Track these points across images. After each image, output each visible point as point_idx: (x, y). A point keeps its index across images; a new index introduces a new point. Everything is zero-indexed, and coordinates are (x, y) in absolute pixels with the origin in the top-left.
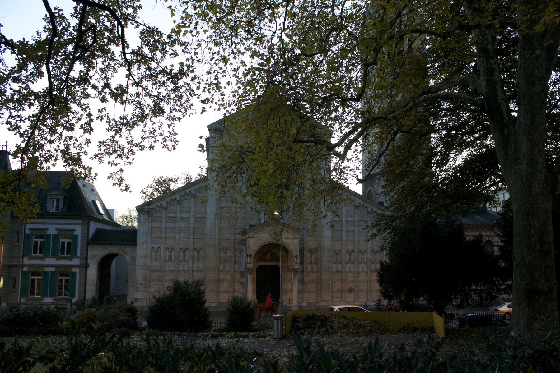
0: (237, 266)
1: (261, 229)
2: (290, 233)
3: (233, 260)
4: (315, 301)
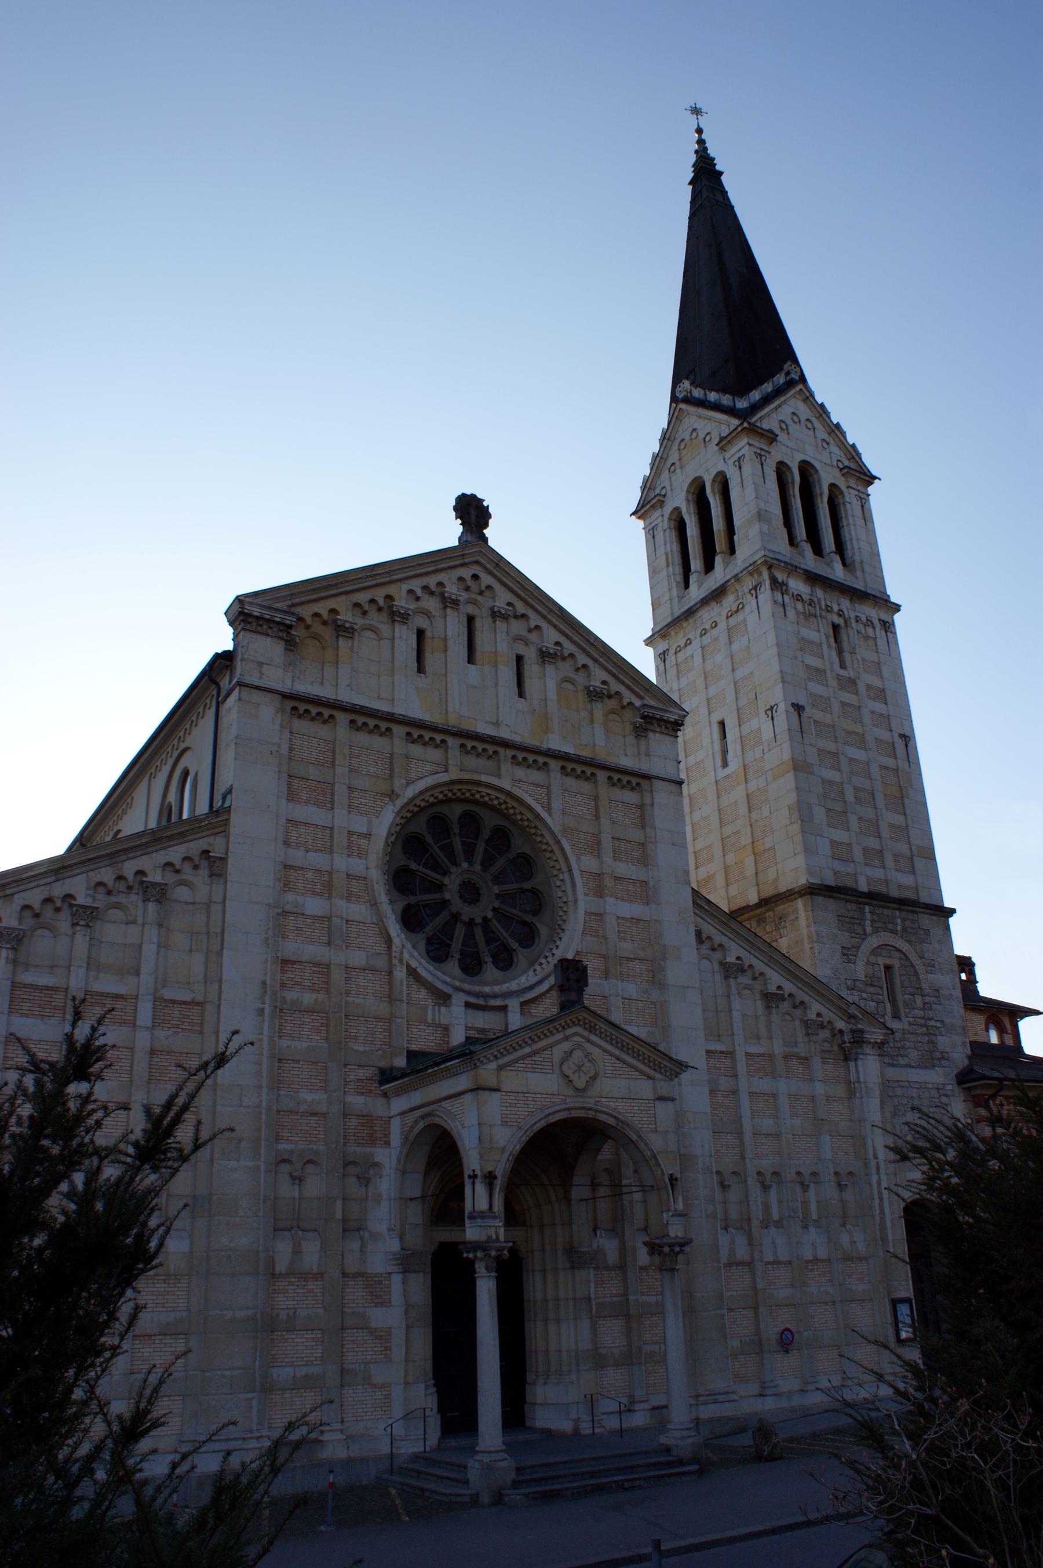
0: (356, 1245)
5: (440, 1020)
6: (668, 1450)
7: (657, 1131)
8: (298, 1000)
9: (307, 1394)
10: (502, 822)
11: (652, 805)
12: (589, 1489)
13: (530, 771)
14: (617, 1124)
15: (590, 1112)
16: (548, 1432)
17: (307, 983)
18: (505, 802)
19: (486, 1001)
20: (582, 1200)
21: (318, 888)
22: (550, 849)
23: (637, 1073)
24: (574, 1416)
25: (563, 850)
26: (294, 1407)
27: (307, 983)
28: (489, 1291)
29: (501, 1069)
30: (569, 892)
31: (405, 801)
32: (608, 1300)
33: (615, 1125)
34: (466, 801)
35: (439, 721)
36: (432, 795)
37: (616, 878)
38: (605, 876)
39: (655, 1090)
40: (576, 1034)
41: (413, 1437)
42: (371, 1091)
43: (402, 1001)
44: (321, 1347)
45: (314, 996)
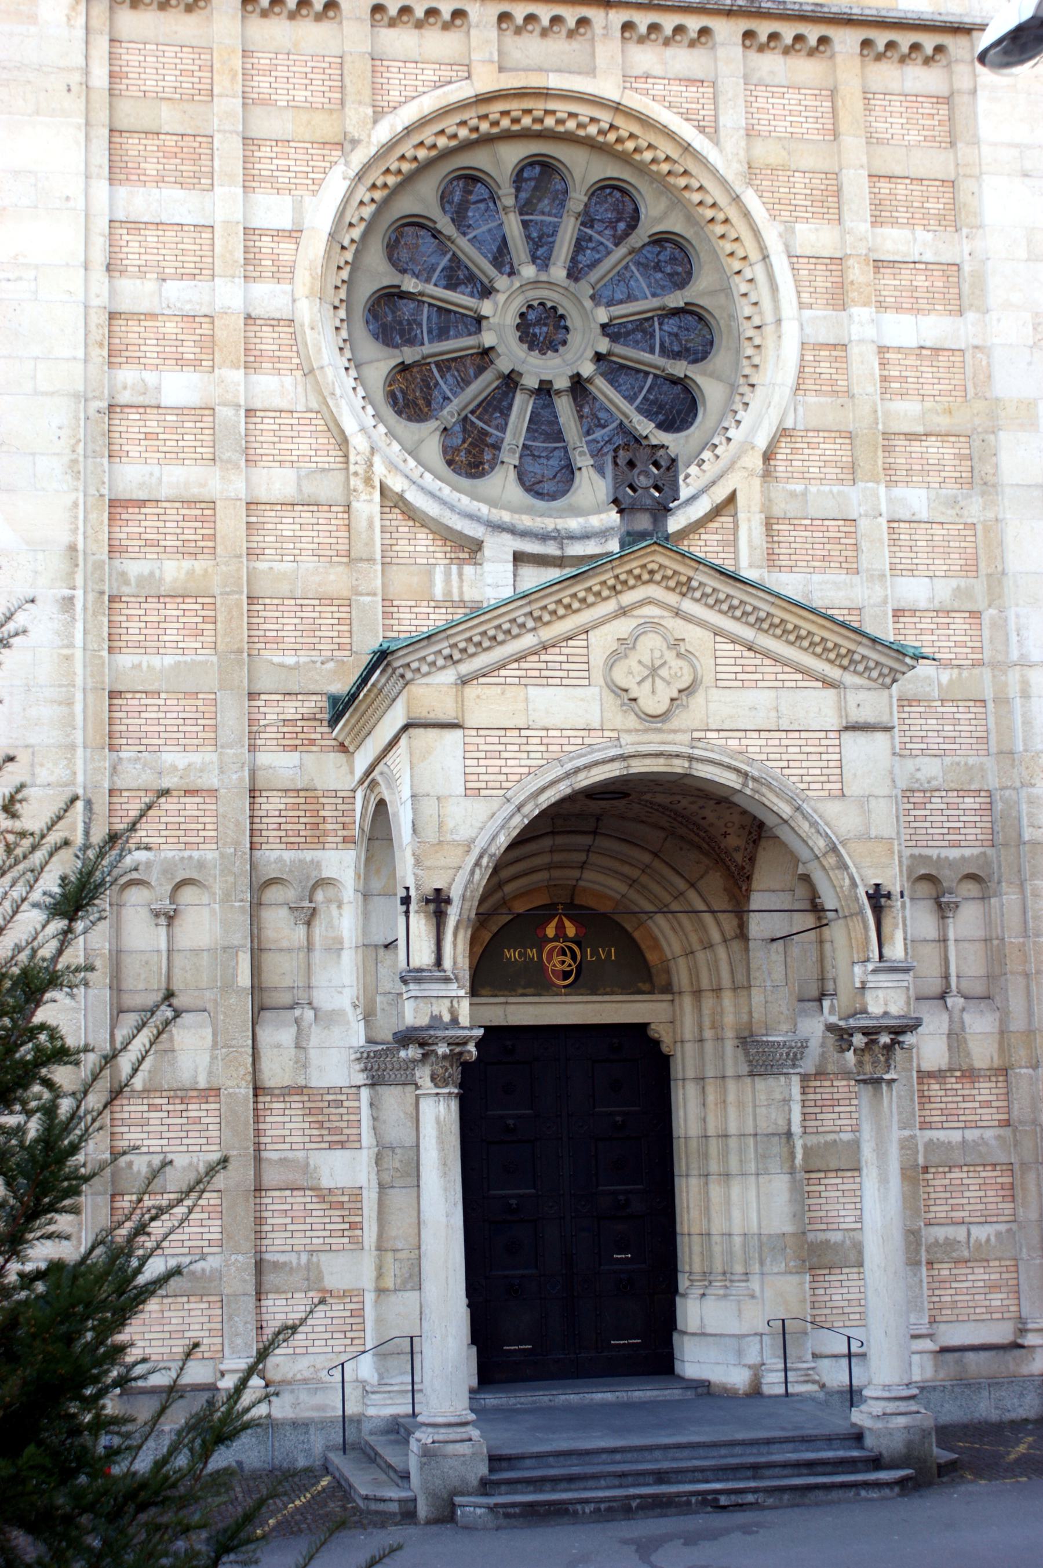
0: (286, 1036)
1: (528, 641)
2: (485, 823)
3: (244, 979)
4: (1000, 1333)
5: (461, 593)
6: (858, 1437)
8: (152, 574)
10: (612, 170)
11: (974, 92)
12: (634, 1504)
13: (670, 52)
14: (745, 785)
15: (677, 762)
16: (704, 1389)
17: (171, 542)
18: (612, 127)
19: (562, 548)
20: (773, 940)
21: (189, 350)
22: (721, 216)
23: (799, 676)
24: (752, 1358)
25: (746, 215)
26: (167, 1328)
27: (171, 542)
28: (438, 1122)
29: (464, 683)
30: (766, 304)
31: (373, 150)
33: (738, 787)
34: (526, 135)
35: (922, 9)
36: (442, 132)
37: (878, 265)
38: (850, 262)
39: (842, 708)
40: (649, 601)
41: (396, 1388)
42: (312, 742)
43: (371, 560)
44: (219, 1222)
45: (187, 564)
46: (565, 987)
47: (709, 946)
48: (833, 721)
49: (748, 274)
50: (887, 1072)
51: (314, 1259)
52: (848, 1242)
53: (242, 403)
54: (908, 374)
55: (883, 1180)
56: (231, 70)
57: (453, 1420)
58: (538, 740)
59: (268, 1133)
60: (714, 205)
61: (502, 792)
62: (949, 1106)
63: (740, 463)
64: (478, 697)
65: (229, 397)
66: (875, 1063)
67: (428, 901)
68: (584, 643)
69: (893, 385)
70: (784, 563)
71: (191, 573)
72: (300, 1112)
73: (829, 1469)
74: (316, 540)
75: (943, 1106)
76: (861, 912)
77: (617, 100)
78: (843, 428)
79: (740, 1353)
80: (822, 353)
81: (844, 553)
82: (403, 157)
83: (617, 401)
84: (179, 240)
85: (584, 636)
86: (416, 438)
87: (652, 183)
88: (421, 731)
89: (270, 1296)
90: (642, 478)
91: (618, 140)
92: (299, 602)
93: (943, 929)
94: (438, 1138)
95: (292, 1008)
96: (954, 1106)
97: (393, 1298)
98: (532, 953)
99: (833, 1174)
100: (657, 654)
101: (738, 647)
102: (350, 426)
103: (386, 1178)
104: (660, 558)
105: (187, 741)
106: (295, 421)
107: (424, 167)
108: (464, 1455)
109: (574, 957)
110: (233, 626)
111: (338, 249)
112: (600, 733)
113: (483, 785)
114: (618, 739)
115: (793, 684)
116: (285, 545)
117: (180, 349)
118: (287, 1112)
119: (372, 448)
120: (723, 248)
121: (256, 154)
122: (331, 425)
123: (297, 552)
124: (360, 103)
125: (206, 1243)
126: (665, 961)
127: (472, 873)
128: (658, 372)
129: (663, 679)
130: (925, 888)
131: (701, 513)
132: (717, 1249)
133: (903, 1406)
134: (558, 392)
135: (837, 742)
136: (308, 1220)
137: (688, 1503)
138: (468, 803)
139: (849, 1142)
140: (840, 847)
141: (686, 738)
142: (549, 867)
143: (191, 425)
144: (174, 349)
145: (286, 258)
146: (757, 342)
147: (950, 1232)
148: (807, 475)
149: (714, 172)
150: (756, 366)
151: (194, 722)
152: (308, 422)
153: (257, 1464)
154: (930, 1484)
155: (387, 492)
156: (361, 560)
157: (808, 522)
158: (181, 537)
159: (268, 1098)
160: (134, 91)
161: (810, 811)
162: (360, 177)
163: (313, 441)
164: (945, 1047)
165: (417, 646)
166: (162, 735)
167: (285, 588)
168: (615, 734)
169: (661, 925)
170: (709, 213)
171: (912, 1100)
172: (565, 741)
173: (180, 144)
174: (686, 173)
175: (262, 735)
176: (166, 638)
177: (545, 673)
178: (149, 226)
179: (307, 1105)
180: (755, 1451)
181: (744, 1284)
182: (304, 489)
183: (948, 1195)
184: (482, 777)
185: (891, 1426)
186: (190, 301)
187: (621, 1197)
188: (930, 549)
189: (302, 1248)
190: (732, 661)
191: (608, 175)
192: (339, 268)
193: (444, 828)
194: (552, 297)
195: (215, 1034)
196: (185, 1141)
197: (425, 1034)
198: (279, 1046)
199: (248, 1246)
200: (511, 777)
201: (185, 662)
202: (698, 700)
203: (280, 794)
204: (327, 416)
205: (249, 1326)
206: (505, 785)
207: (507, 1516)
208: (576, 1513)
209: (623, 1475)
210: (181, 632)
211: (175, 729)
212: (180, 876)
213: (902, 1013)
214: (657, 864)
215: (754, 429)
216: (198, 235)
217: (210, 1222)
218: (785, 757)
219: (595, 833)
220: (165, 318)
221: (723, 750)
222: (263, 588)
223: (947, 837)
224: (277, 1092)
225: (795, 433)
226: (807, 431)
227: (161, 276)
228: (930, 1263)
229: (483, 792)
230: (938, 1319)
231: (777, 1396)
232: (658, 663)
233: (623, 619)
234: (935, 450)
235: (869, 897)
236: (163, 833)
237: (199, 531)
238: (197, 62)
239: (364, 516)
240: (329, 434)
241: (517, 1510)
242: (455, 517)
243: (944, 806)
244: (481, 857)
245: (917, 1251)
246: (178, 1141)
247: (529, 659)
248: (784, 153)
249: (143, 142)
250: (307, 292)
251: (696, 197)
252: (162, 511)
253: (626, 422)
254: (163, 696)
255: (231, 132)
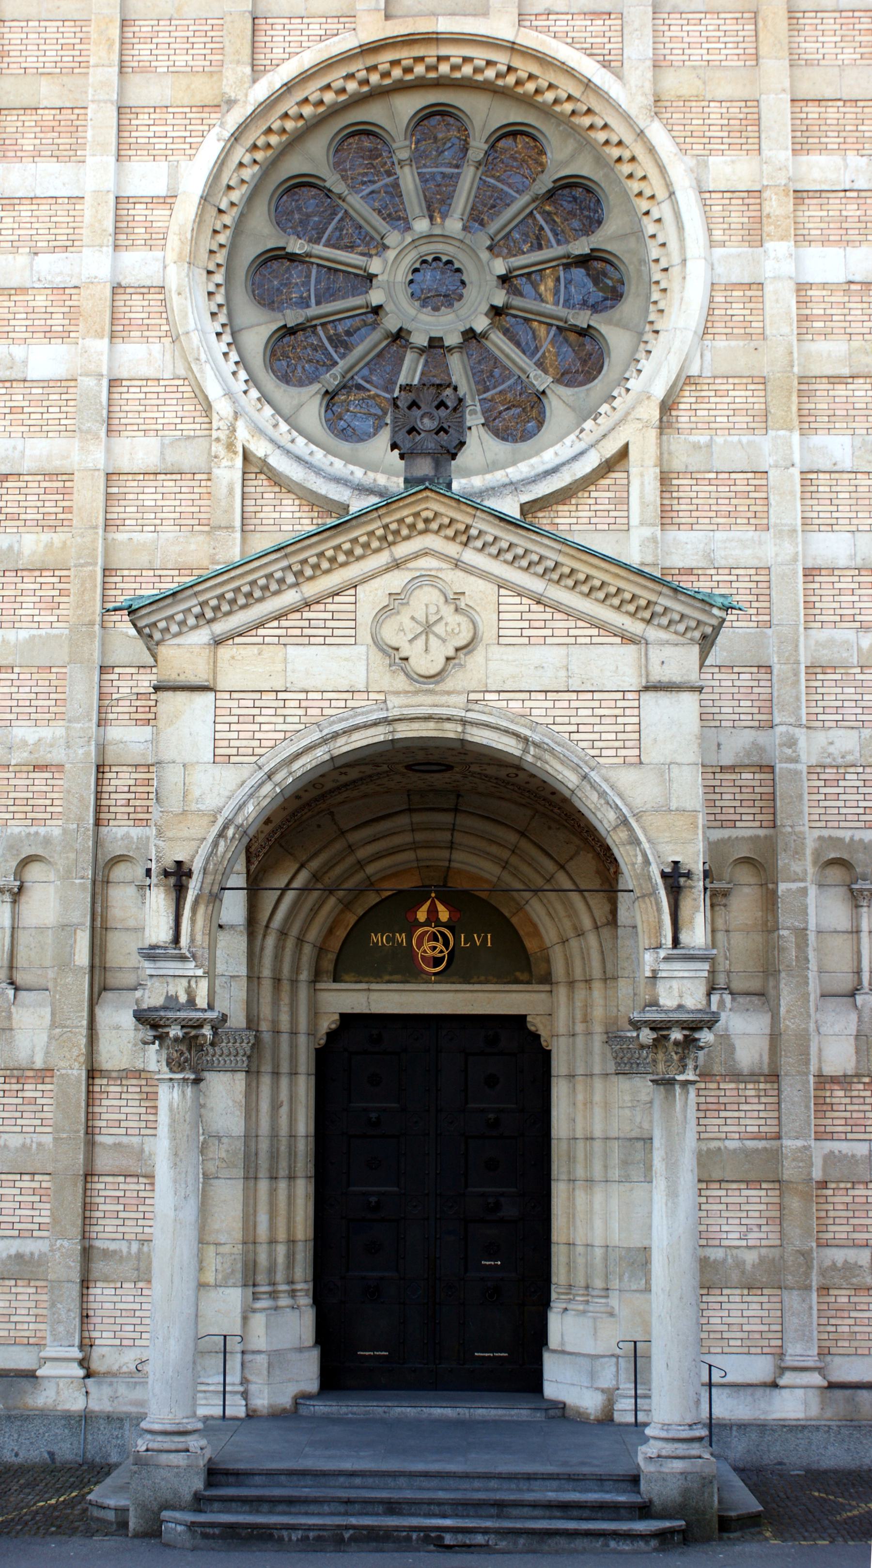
1: (290, 597)
3: (82, 957)
7: (641, 763)
9: (19, 1290)
10: (515, 115)
12: (347, 1535)
15: (448, 726)
16: (560, 1408)
18: (510, 69)
21: (58, 322)
22: (627, 155)
23: (595, 632)
24: (606, 1379)
25: (651, 150)
28: (171, 1109)
32: (732, 1145)
33: (518, 753)
34: (421, 84)
36: (328, 87)
37: (800, 195)
40: (425, 553)
43: (230, 528)
45: (46, 537)
46: (435, 974)
47: (580, 934)
48: (631, 680)
49: (655, 214)
50: (682, 1072)
51: (145, 1249)
52: (730, 1260)
53: (105, 372)
54: (833, 312)
55: (672, 1193)
56: (109, 39)
57: (169, 1428)
58: (296, 703)
59: (104, 1116)
60: (620, 143)
61: (254, 759)
62: (855, 1115)
63: (636, 414)
64: (233, 658)
65: (92, 367)
66: (668, 1061)
67: (166, 874)
68: (352, 599)
69: (815, 324)
70: (683, 521)
71: (49, 546)
72: (137, 1096)
73: (586, 1513)
74: (178, 509)
75: (848, 1115)
76: (654, 893)
77: (511, 39)
78: (756, 374)
79: (593, 1375)
80: (735, 293)
81: (752, 508)
82: (286, 115)
83: (513, 356)
84: (53, 213)
85: (352, 592)
86: (295, 402)
87: (558, 125)
88: (169, 694)
89: (99, 1284)
90: (426, 420)
91: (518, 83)
92: (158, 573)
93: (856, 919)
94: (170, 1126)
95: (136, 989)
96: (861, 1115)
97: (213, 1294)
98: (401, 938)
99: (717, 1185)
100: (433, 609)
101: (525, 601)
102: (214, 391)
103: (211, 1168)
104: (434, 505)
105: (39, 716)
106: (162, 389)
107: (313, 126)
108: (178, 1467)
109: (446, 943)
110: (86, 597)
111: (214, 212)
112: (365, 696)
113: (234, 751)
114: (385, 701)
115: (588, 640)
116: (146, 516)
117: (49, 322)
118: (124, 1096)
119: (236, 413)
120: (631, 189)
121: (133, 122)
122: (197, 391)
123: (158, 522)
124: (238, 62)
125: (36, 1227)
126: (544, 949)
127: (215, 844)
128: (561, 324)
129: (437, 636)
130: (836, 874)
131: (588, 469)
132: (581, 1260)
133: (681, 1449)
134: (450, 349)
135: (636, 704)
136: (141, 1208)
137: (408, 1539)
138: (217, 770)
139: (735, 1150)
140: (632, 821)
141: (461, 700)
142: (415, 846)
143: (57, 397)
144: (42, 322)
145: (159, 224)
146: (663, 285)
147: (851, 1255)
148: (712, 425)
149: (616, 107)
150: (662, 311)
151: (46, 696)
152: (175, 389)
153: (69, 1456)
154: (707, 1540)
155: (251, 458)
156: (220, 528)
157: (713, 475)
158: (41, 510)
159: (105, 1081)
160: (15, 69)
161: (598, 779)
162: (236, 137)
163: (179, 408)
164: (852, 1050)
165: (161, 604)
166: (14, 710)
167: (143, 559)
168: (381, 697)
169: (536, 909)
170: (615, 152)
171: (807, 1107)
172: (326, 704)
173: (57, 117)
174: (589, 111)
175: (114, 709)
176: (22, 612)
177: (306, 632)
178: (24, 201)
179: (145, 1089)
180: (513, 1486)
181: (603, 1300)
182: (167, 457)
183: (851, 1214)
184: (233, 743)
185: (665, 1470)
186: (61, 273)
187: (491, 1200)
188: (853, 502)
189: (133, 1236)
190: (518, 616)
191: (512, 120)
192: (215, 232)
193: (190, 797)
194: (446, 250)
195: (53, 1014)
196: (19, 1122)
197: (155, 1015)
198: (118, 1028)
199: (76, 1231)
200: (264, 743)
201: (40, 636)
202: (476, 660)
203: (130, 769)
204: (193, 383)
205: (73, 1315)
206: (258, 751)
207: (205, 1536)
208: (281, 1539)
209: (348, 1502)
210: (38, 606)
211: (28, 703)
212: (26, 852)
213: (699, 1007)
214: (524, 844)
215: (651, 380)
216: (71, 207)
217: (41, 1205)
218: (574, 720)
219: (456, 810)
220: (35, 292)
221: (503, 713)
222: (120, 559)
223: (862, 818)
224: (114, 1075)
225: (701, 381)
226: (715, 377)
227: (33, 250)
228: (824, 1289)
229: (233, 759)
230: (832, 1351)
231: (627, 1425)
232: (432, 619)
233: (396, 572)
234: (863, 393)
235: (664, 875)
236: (11, 809)
237: (59, 504)
238: (79, 35)
239: (225, 483)
240: (195, 401)
241: (217, 1531)
242: (320, 481)
243: (861, 783)
244: (225, 827)
245: (807, 1275)
246: (13, 1122)
247: (290, 616)
248: (699, 83)
249: (22, 118)
250: (175, 258)
251: (601, 136)
252: (24, 484)
253: (524, 377)
254: (16, 670)
255: (105, 102)
